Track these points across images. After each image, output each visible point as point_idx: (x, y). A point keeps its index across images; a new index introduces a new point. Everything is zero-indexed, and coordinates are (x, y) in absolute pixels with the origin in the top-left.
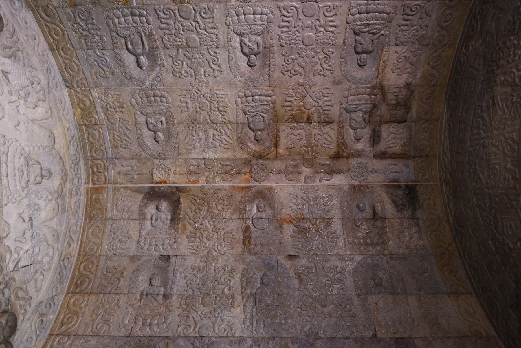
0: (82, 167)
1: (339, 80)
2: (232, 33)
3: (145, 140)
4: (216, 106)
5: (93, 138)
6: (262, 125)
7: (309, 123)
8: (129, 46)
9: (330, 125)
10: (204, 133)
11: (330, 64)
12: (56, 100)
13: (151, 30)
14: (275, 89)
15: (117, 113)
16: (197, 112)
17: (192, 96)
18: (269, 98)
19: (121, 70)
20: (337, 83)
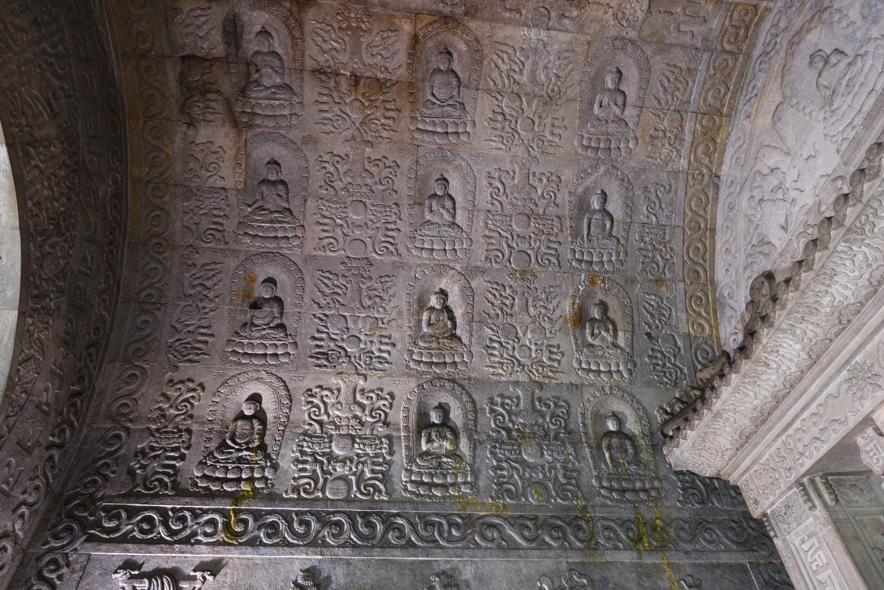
0: (761, 44)
1: (307, 143)
2: (465, 228)
3: (637, 78)
4: (507, 123)
5: (720, 91)
6: (436, 82)
7: (356, 76)
8: (608, 224)
9: (319, 68)
10: (537, 78)
11: (325, 172)
12: (742, 166)
13: (573, 242)
14: (409, 140)
15: (663, 128)
16: (540, 117)
17: (541, 143)
18: (421, 126)
19: (632, 193)
20: (309, 140)
